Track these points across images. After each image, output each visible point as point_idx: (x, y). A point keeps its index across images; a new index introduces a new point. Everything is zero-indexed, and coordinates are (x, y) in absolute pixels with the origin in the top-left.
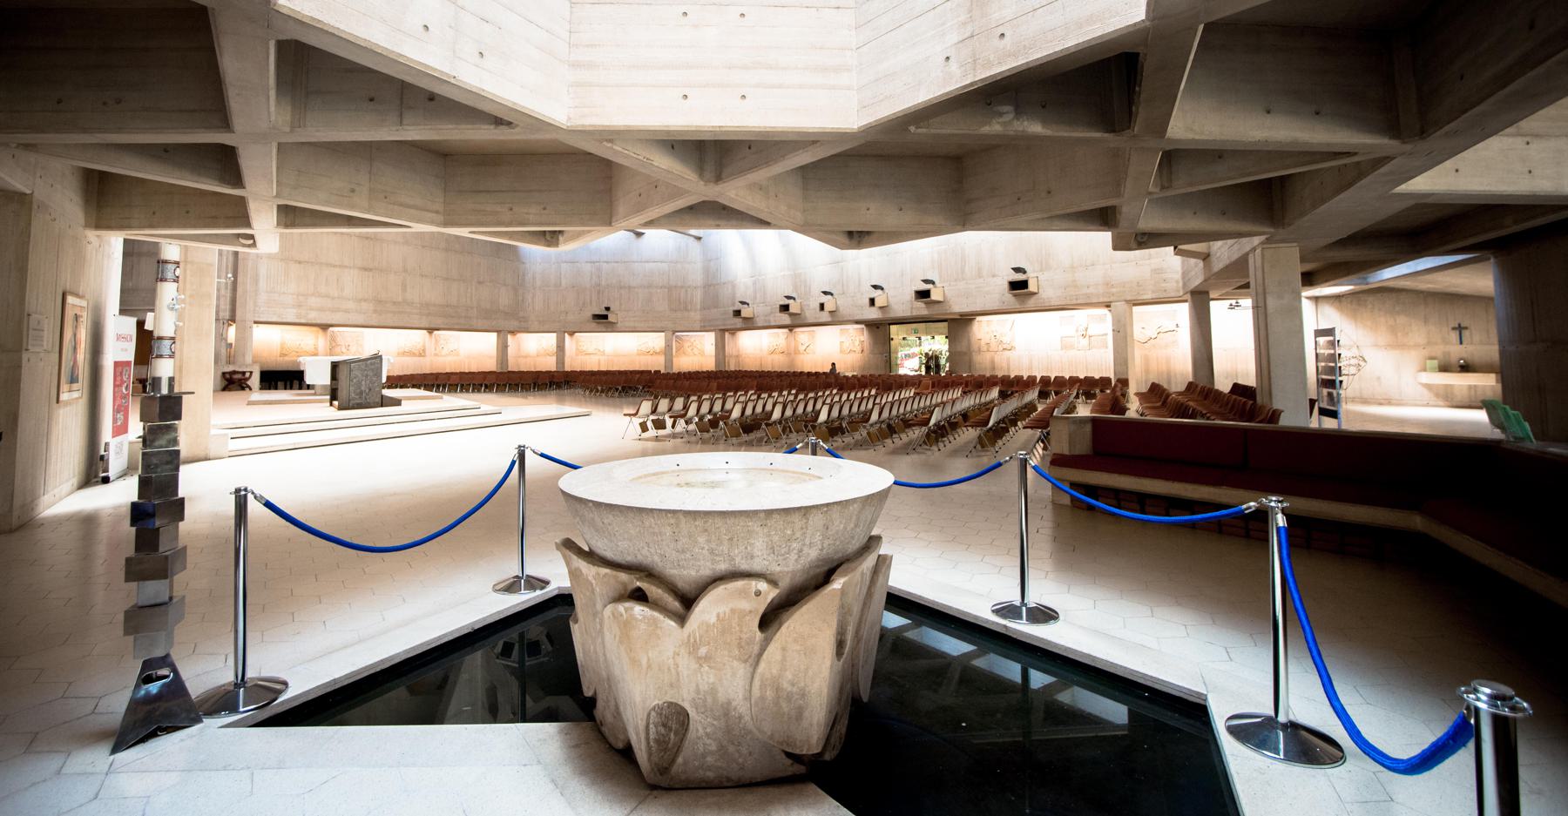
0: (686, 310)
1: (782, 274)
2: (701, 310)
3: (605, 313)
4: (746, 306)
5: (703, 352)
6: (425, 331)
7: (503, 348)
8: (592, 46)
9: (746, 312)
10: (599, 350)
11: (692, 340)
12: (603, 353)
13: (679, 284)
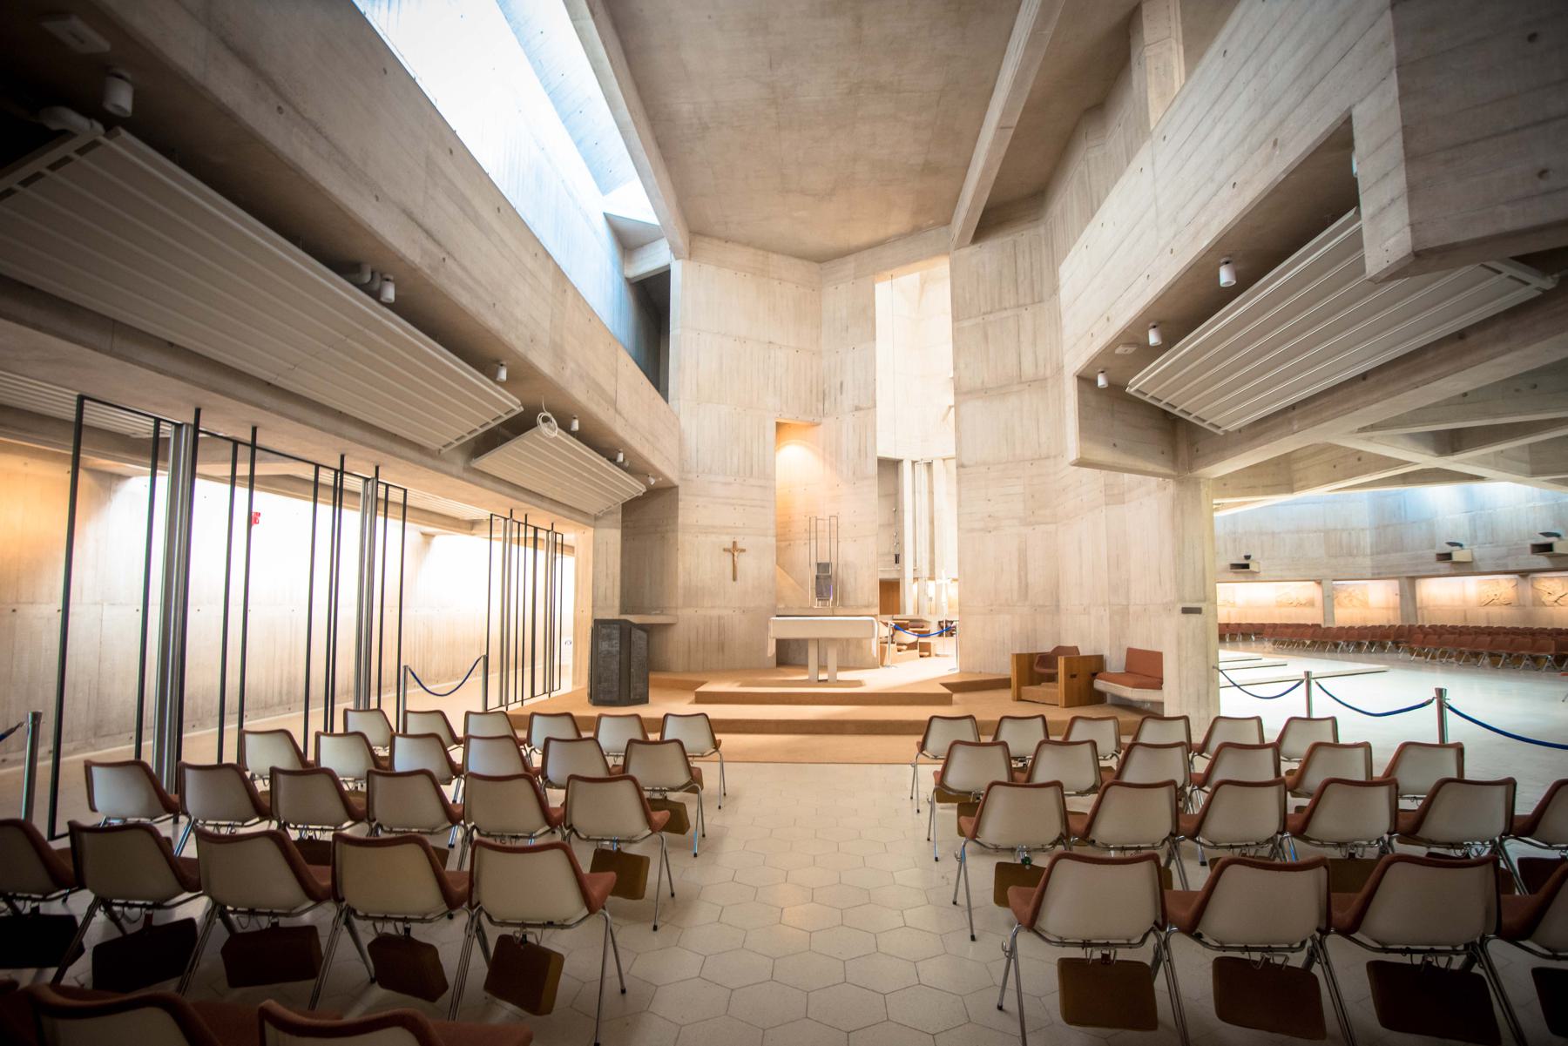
0: (1351, 555)
1: (1532, 505)
2: (1372, 554)
3: (1245, 562)
4: (1458, 548)
5: (1234, 603)
6: (1313, 583)
7: (1329, 600)
8: (1196, 192)
9: (1458, 555)
10: (1229, 602)
11: (1350, 589)
12: (1234, 605)
13: (1339, 527)
